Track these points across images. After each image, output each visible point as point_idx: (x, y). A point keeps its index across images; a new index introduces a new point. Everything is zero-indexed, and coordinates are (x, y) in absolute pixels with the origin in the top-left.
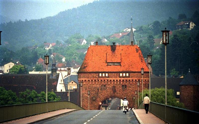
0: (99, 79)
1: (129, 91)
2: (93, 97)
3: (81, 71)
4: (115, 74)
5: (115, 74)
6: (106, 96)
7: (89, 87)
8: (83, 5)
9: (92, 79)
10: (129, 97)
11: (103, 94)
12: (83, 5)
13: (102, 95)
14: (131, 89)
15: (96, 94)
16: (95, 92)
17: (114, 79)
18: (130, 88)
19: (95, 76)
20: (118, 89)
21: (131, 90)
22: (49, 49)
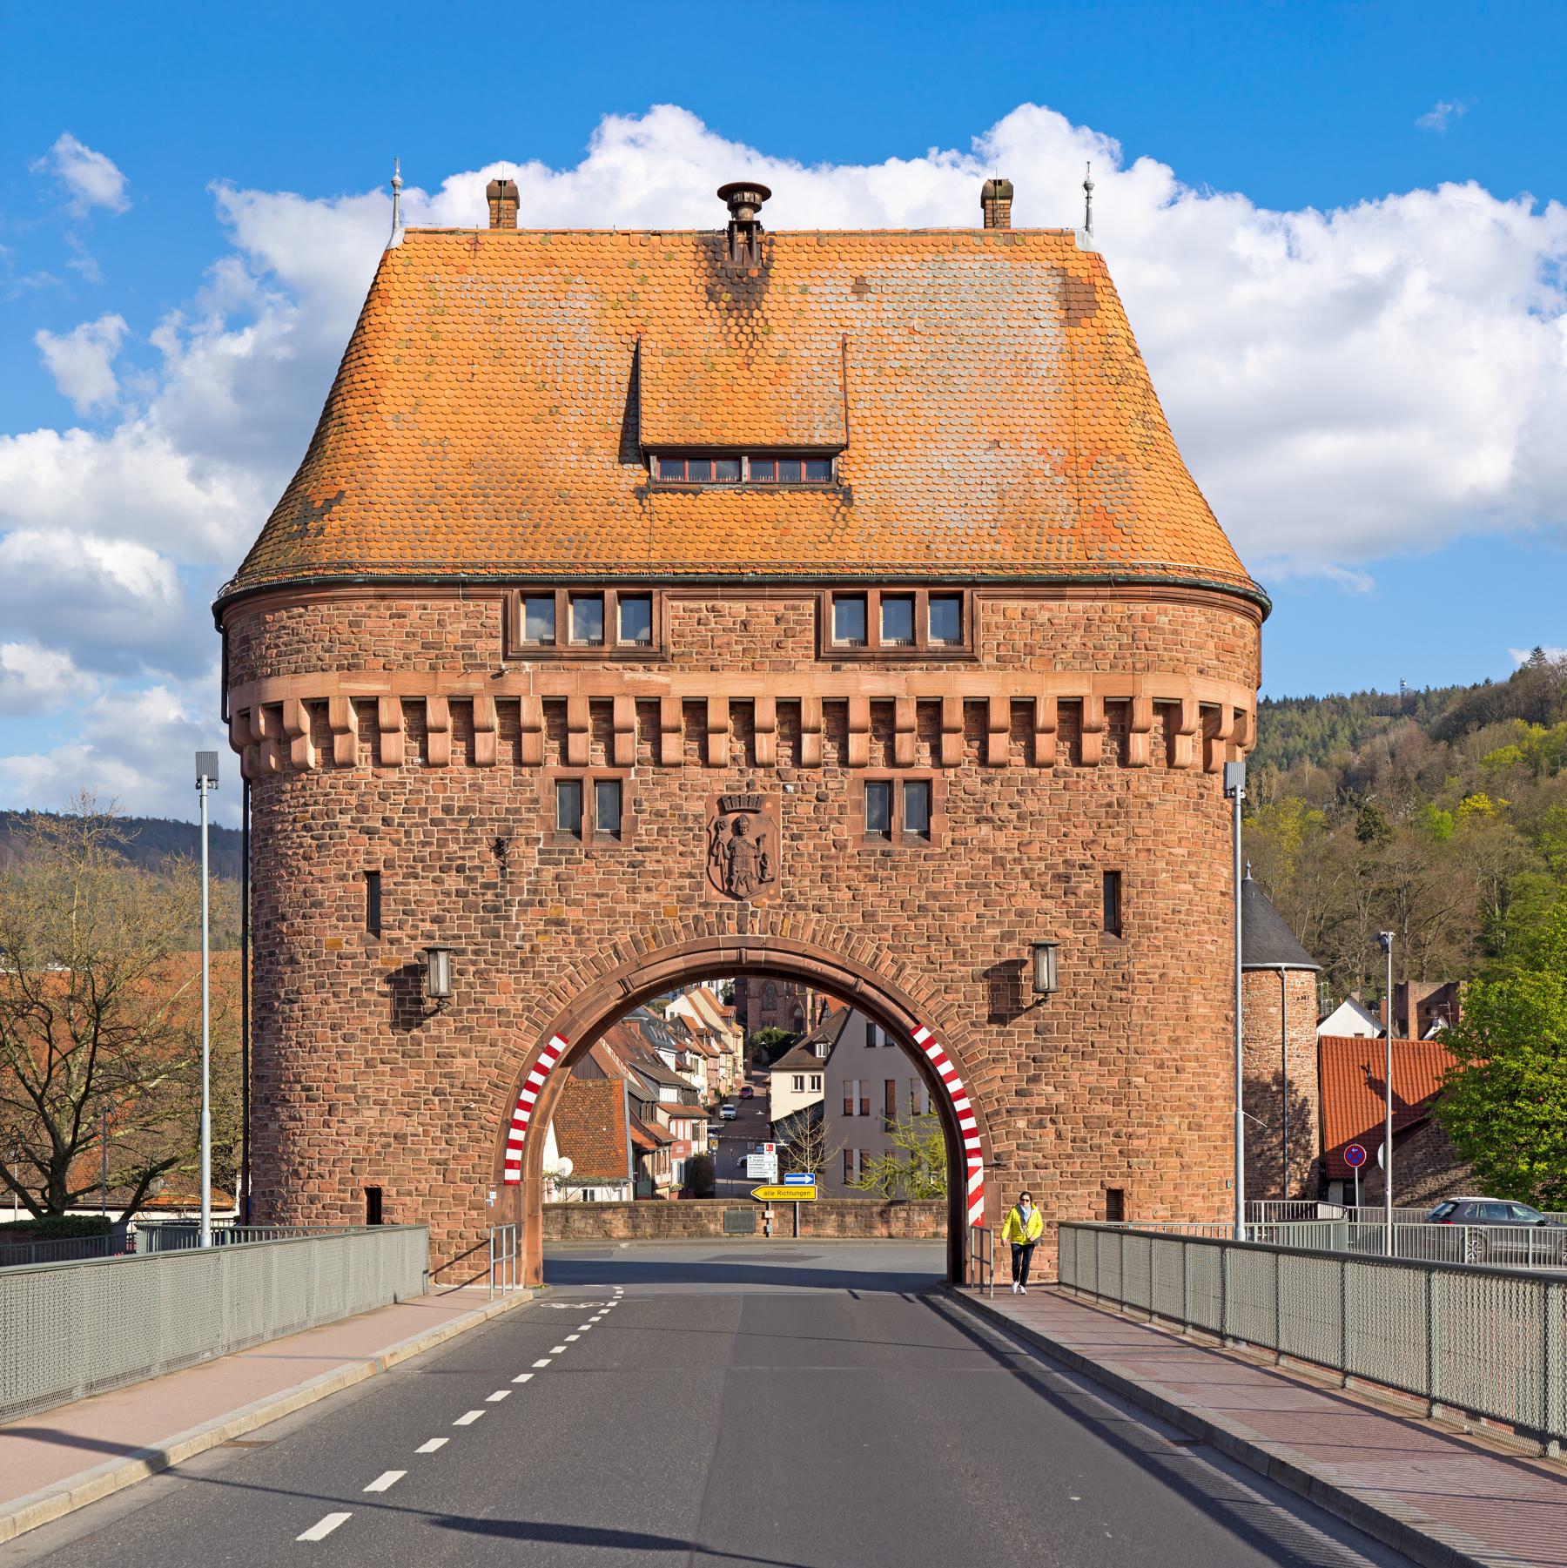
0: (514, 686)
1: (963, 867)
2: (432, 951)
3: (285, 563)
4: (765, 611)
5: (758, 605)
6: (623, 938)
7: (362, 808)
8: (1368, 692)
9: (413, 686)
10: (959, 954)
11: (572, 914)
12: (1368, 692)
13: (559, 923)
14: (1001, 840)
15: (470, 907)
16: (453, 882)
17: (742, 686)
18: (985, 829)
19: (454, 632)
20: (807, 845)
21: (999, 862)
22: (1530, 724)
